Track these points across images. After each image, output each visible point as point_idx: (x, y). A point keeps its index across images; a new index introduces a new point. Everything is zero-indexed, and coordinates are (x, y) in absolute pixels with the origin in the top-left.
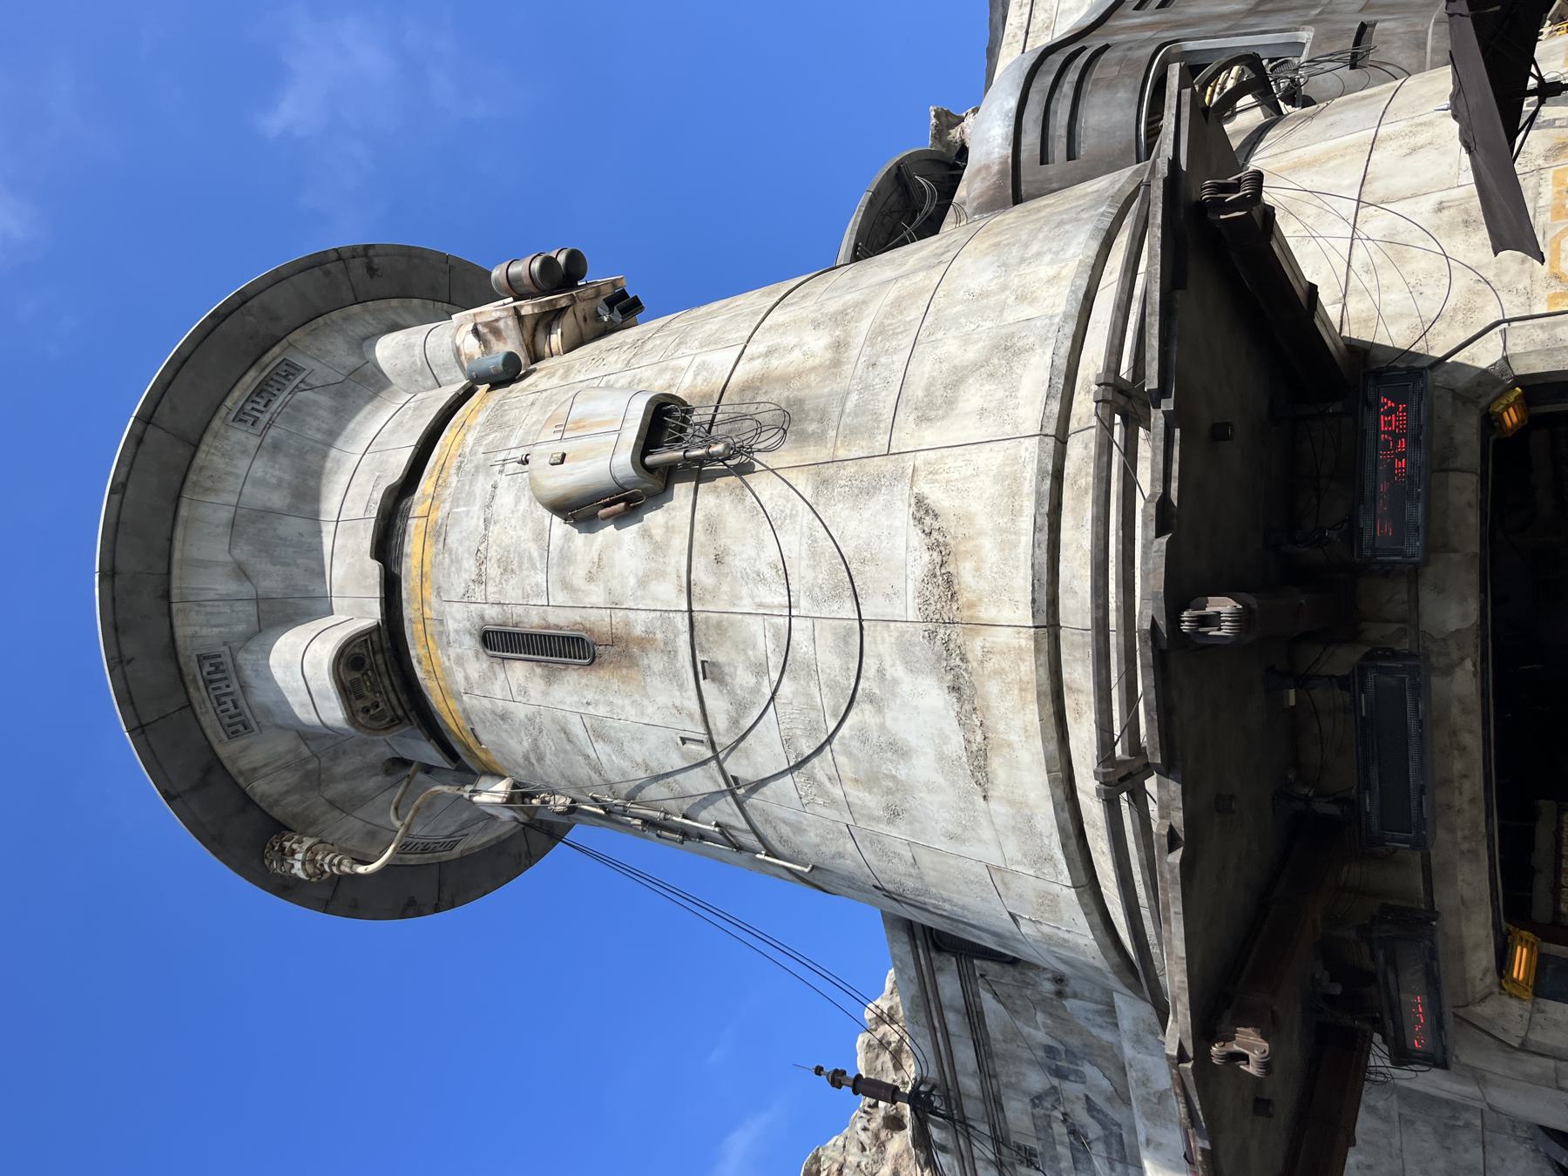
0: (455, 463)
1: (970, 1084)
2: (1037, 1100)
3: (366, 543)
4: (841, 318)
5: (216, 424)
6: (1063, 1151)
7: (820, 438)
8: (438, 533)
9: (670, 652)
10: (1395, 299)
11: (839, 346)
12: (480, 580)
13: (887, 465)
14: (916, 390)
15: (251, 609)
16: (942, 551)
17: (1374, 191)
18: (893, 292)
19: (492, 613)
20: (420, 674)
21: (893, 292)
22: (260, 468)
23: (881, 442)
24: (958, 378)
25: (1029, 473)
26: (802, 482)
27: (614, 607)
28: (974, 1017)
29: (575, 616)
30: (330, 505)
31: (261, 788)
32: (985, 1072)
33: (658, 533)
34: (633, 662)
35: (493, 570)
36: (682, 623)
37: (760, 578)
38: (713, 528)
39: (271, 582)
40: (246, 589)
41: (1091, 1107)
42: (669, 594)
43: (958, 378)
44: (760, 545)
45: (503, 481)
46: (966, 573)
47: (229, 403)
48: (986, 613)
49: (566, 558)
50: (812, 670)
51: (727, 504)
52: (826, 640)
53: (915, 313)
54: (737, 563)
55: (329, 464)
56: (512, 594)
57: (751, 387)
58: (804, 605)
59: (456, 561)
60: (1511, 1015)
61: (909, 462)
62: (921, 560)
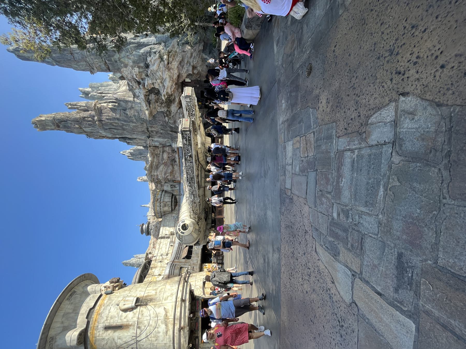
0: (103, 305)
3: (86, 316)
4: (156, 290)
5: (64, 301)
8: (99, 314)
9: (134, 326)
10: (198, 293)
11: (156, 293)
12: (107, 320)
13: (162, 305)
14: (164, 298)
17: (196, 285)
18: (161, 288)
19: (107, 324)
20: (89, 334)
21: (161, 288)
23: (161, 302)
26: (153, 306)
27: (128, 321)
29: (121, 323)
33: (135, 312)
35: (109, 318)
36: (136, 322)
37: (147, 316)
38: (142, 311)
42: (135, 319)
44: (148, 313)
45: (112, 307)
46: (168, 314)
48: (169, 318)
49: (121, 316)
51: (144, 308)
53: (163, 290)
54: (144, 315)
56: (112, 321)
57: (146, 296)
58: (152, 319)
59: (103, 318)
61: (164, 304)
62: (164, 313)
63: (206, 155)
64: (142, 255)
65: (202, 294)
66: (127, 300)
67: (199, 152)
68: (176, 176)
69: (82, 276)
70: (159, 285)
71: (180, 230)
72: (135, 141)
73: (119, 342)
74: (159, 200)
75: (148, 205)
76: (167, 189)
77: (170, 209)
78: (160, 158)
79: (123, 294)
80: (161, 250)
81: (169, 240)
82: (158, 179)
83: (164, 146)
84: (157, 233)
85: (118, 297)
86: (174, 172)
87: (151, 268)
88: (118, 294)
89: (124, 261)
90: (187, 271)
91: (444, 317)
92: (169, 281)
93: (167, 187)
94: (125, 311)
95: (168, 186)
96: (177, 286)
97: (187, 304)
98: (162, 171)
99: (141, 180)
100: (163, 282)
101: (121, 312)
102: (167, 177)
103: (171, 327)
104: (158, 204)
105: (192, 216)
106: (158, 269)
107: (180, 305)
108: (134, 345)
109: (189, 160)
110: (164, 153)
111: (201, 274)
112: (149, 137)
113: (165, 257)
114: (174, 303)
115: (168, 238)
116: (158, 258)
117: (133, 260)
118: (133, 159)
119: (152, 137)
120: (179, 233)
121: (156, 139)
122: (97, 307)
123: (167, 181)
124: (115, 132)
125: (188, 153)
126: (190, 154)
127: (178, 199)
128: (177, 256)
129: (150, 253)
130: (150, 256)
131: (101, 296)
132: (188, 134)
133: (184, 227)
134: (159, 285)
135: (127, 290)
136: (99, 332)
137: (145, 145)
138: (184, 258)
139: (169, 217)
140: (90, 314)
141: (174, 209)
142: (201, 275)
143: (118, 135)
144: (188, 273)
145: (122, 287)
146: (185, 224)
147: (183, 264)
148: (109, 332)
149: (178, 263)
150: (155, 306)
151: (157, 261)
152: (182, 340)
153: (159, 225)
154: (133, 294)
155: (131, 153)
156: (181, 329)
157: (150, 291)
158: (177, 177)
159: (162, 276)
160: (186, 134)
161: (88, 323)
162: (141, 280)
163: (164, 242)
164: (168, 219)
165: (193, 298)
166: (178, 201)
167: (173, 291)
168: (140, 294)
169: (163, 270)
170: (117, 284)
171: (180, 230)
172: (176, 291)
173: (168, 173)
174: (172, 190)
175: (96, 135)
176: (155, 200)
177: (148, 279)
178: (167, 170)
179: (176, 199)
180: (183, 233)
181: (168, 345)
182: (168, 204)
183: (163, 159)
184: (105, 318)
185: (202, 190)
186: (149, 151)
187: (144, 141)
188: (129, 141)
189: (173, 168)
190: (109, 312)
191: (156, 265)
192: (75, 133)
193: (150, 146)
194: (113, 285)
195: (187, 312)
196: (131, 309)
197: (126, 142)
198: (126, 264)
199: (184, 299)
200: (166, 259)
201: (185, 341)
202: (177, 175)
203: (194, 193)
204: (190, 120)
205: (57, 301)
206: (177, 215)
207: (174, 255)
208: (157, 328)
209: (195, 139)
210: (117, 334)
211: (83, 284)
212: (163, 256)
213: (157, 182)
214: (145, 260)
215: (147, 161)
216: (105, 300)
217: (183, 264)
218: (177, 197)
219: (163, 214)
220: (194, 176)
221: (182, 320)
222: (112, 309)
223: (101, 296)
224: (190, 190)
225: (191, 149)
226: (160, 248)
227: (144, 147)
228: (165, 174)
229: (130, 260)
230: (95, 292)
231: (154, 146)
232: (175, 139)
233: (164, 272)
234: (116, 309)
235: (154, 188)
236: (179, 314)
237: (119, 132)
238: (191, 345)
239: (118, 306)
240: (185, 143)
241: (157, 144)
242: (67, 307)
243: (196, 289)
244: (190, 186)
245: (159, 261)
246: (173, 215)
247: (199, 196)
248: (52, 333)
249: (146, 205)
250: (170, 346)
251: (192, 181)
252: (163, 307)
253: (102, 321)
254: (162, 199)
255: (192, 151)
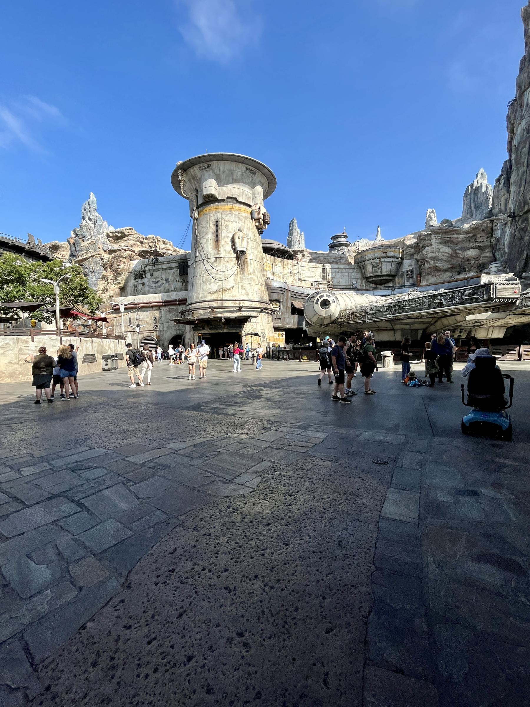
1: (160, 267)
2: (161, 276)
3: (229, 196)
4: (254, 272)
5: (246, 165)
6: (155, 280)
7: (240, 274)
9: (218, 254)
13: (237, 283)
14: (244, 285)
15: (218, 173)
16: (229, 290)
17: (257, 324)
18: (256, 279)
19: (220, 223)
20: (212, 205)
21: (256, 279)
22: (239, 173)
24: (245, 289)
25: (236, 298)
27: (222, 245)
28: (171, 268)
29: (221, 239)
30: (235, 185)
31: (191, 170)
32: (163, 269)
33: (230, 252)
34: (216, 248)
35: (226, 223)
36: (221, 256)
38: (231, 260)
39: (222, 176)
40: (221, 172)
41: (162, 284)
42: (224, 254)
43: (245, 289)
46: (227, 292)
47: (249, 166)
48: (223, 294)
50: (217, 274)
51: (234, 262)
52: (221, 276)
55: (240, 184)
56: (223, 227)
57: (247, 262)
58: (223, 273)
60: (196, 334)
61: (237, 285)
62: (228, 287)
63: (455, 329)
64: (304, 243)
65: (247, 333)
66: (243, 240)
67: (459, 318)
68: (430, 277)
69: (273, 176)
70: (259, 276)
71: (321, 297)
72: (503, 191)
73: (203, 241)
74: (384, 255)
75: (379, 237)
76: (404, 264)
77: (369, 275)
78: (467, 245)
79: (251, 232)
80: (306, 270)
81: (321, 280)
82: (424, 247)
83: (494, 248)
84: (333, 260)
85: (247, 228)
86: (437, 274)
87: (283, 261)
88: (251, 227)
89: (297, 220)
90: (275, 311)
91: (136, 471)
92: (264, 288)
93: (408, 265)
94: (233, 240)
95: (411, 265)
96: (257, 299)
97: (237, 314)
98: (439, 252)
99: (430, 216)
100: (262, 281)
101: (231, 236)
102: (428, 262)
103: (214, 297)
104: (377, 255)
105: (345, 312)
106: (281, 270)
107: (236, 305)
108: (201, 258)
109: (433, 302)
110: (477, 250)
111: (270, 329)
112: (513, 216)
113: (297, 278)
114: (237, 298)
115: (324, 278)
116: (296, 267)
117: (297, 232)
118: (466, 195)
119: (511, 223)
120: (318, 297)
121: (508, 230)
122: (237, 206)
123: (420, 263)
124: (523, 150)
125: (447, 299)
126: (444, 303)
127: (386, 285)
128: (296, 295)
129: (303, 255)
130: (299, 256)
131: (250, 206)
132: (482, 298)
133: (325, 304)
134: (259, 276)
135: (255, 237)
136: (214, 216)
137: (495, 211)
138: (292, 304)
139: (356, 275)
140: (232, 200)
141: (369, 282)
142: (269, 329)
143: (516, 158)
144: (273, 311)
145: (258, 228)
146: (330, 303)
147: (285, 305)
148: (213, 227)
149: (286, 297)
150: (236, 275)
151: (291, 268)
152: (202, 312)
153: (343, 261)
154: (250, 246)
155: (478, 188)
156: (212, 309)
157: (252, 266)
158: (427, 280)
159: (271, 277)
160: (483, 293)
161: (223, 201)
162: (266, 250)
163: (317, 274)
164: (353, 274)
165: (243, 321)
166: (383, 286)
167: (251, 294)
168: (250, 254)
169: (280, 277)
170: (262, 222)
171: (321, 297)
172: (252, 299)
173: (434, 263)
174: (403, 274)
175: (515, 116)
176: (384, 249)
177: (269, 259)
178: (442, 260)
179: (387, 281)
180: (317, 302)
181: (199, 296)
182: (378, 270)
183: (465, 249)
184: (226, 219)
185: (388, 325)
186: (481, 222)
187: (503, 208)
188: (502, 182)
189: (446, 271)
190: (232, 222)
191: (286, 267)
192: (519, 76)
193: (492, 221)
194: (261, 218)
195: (226, 315)
196: (234, 248)
197: (501, 176)
198: (292, 224)
199: (242, 309)
200: (294, 279)
201: (201, 315)
202: (432, 279)
203: (379, 314)
204: (516, 298)
205: (246, 158)
206: (359, 287)
207: (296, 289)
208: (215, 281)
209: (478, 310)
210: (211, 236)
211: (264, 180)
212: (298, 275)
213: (418, 248)
214: (293, 251)
215: (463, 221)
216: (245, 212)
217: (285, 305)
218: (390, 284)
219: (361, 264)
220: (406, 312)
221: (221, 310)
222: (235, 225)
223: (250, 206)
224: (382, 307)
225: (454, 305)
226: (310, 269)
227: (491, 210)
228: (433, 258)
229: (297, 228)
230: (254, 198)
231: (492, 229)
232: (509, 267)
233: (278, 279)
234: (234, 229)
235: (408, 243)
236: (226, 305)
237: (523, 157)
238: (196, 322)
239: (238, 231)
240: (465, 293)
241: (498, 233)
242: (240, 170)
243: (252, 323)
244: (389, 306)
245: (291, 270)
246: (359, 281)
247: (375, 322)
248: (215, 164)
249: (379, 233)
250: (198, 298)
251: (398, 309)
252: (235, 285)
253: (224, 216)
254: (387, 260)
255: (450, 306)
